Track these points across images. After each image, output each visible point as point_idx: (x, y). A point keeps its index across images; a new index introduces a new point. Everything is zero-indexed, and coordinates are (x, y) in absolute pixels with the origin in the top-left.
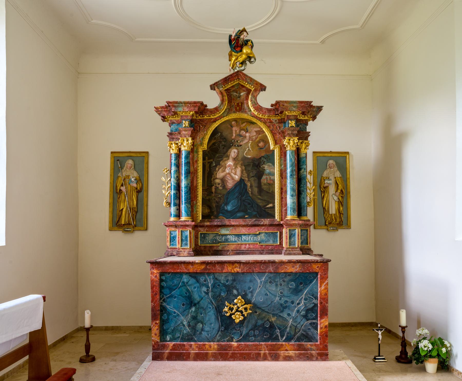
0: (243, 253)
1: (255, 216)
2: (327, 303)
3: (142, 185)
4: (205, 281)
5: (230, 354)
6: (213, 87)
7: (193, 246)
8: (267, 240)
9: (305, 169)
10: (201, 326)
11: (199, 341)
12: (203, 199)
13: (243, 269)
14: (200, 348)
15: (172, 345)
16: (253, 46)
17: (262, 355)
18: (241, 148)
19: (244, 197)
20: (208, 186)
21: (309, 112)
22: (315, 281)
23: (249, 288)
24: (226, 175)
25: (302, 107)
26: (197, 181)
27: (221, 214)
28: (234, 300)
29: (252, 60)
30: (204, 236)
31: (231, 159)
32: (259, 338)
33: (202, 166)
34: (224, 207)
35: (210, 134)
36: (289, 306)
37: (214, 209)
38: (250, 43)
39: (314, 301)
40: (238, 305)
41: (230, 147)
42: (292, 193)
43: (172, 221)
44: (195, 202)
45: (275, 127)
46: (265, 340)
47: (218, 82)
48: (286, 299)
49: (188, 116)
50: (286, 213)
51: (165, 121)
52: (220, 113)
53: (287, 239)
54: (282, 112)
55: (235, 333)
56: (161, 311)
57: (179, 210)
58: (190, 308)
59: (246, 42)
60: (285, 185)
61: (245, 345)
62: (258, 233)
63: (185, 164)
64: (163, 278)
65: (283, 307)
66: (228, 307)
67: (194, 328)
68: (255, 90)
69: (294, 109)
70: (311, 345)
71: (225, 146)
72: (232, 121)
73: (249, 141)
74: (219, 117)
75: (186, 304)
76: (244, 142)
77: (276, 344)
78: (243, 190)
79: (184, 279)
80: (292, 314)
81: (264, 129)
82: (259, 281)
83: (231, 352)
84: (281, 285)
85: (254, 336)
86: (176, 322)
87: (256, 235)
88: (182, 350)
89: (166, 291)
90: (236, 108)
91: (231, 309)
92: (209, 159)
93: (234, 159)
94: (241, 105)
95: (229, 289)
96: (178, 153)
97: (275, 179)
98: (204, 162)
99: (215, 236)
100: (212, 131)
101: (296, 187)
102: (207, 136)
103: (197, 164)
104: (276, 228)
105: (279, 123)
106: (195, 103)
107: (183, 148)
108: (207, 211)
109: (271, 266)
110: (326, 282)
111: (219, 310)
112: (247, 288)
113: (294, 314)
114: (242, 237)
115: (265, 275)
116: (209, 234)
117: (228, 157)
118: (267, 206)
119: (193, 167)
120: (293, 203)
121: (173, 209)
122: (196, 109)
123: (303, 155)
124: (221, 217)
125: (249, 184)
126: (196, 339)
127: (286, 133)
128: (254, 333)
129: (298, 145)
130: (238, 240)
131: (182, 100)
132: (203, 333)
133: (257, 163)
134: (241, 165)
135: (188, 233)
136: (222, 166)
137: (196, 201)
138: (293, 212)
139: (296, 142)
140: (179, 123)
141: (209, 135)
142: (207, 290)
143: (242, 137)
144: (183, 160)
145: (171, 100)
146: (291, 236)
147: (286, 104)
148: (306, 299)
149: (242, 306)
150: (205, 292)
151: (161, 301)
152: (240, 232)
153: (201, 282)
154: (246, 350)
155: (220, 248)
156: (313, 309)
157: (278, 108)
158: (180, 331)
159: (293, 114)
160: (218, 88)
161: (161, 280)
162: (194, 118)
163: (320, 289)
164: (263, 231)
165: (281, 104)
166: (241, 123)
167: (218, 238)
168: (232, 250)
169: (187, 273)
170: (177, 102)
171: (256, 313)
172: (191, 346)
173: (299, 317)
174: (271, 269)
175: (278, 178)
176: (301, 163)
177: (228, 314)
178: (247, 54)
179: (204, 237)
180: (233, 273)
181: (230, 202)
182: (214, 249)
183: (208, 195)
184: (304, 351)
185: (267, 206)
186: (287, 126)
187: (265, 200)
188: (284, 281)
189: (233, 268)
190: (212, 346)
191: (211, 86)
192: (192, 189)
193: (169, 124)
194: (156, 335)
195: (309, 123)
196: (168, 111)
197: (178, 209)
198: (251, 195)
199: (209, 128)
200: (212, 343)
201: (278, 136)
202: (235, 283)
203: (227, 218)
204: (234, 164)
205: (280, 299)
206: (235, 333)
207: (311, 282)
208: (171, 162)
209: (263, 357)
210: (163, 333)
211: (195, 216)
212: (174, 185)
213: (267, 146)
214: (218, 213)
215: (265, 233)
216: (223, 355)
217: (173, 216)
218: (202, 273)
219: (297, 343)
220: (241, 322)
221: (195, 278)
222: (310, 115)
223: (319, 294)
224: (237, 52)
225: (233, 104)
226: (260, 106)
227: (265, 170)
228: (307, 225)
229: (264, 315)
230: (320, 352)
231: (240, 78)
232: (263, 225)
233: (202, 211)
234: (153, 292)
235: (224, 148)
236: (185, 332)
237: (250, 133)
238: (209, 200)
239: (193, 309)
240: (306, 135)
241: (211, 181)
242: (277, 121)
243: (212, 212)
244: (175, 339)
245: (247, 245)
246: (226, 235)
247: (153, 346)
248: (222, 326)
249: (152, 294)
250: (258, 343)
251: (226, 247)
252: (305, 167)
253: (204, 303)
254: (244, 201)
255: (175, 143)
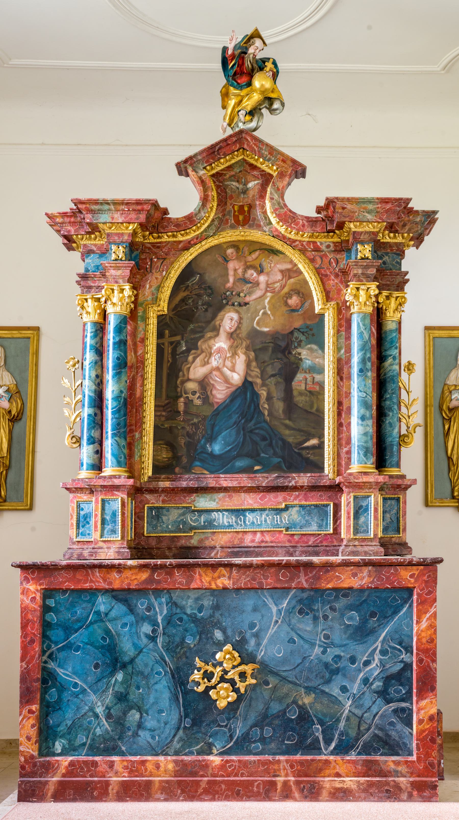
0: (247, 552)
1: (277, 468)
2: (434, 661)
3: (23, 404)
4: (149, 609)
5: (203, 785)
6: (183, 168)
7: (130, 535)
8: (303, 522)
9: (394, 358)
10: (137, 716)
11: (131, 754)
12: (156, 427)
13: (238, 580)
14: (132, 769)
15: (66, 764)
16: (278, 72)
17: (279, 786)
18: (248, 310)
19: (253, 422)
20: (168, 397)
21: (404, 225)
22: (405, 609)
23: (252, 626)
24: (211, 373)
25: (387, 211)
26: (143, 385)
27: (198, 463)
28: (215, 653)
29: (276, 105)
30: (157, 514)
31: (223, 335)
32: (273, 745)
33: (155, 351)
34: (204, 447)
36: (344, 668)
37: (183, 452)
38: (269, 65)
39: (404, 656)
40: (225, 665)
41: (220, 308)
42: (363, 411)
43: (82, 479)
44: (137, 435)
45: (326, 261)
46: (288, 751)
47: (195, 155)
48: (337, 651)
49: (122, 234)
50: (349, 459)
51: (73, 249)
52: (198, 228)
53: (349, 518)
54: (341, 226)
55: (216, 733)
56: (44, 681)
57: (100, 453)
58: (112, 674)
59: (261, 65)
60: (348, 394)
61: (240, 761)
62: (283, 506)
63: (117, 344)
64: (51, 603)
65: (331, 671)
66: (202, 672)
67: (119, 722)
68: (281, 175)
69: (369, 217)
70: (397, 763)
71: (209, 305)
72: (228, 248)
73: (264, 294)
75: (104, 663)
76: (254, 296)
77: (312, 760)
78: (249, 407)
79: (100, 604)
80: (352, 688)
81: (300, 266)
82: (274, 609)
83: (206, 779)
84: (326, 617)
85: (263, 740)
86: (78, 708)
87: (279, 511)
88: (91, 776)
89: (56, 634)
90: (236, 218)
91: (208, 676)
93: (231, 336)
94: (249, 211)
95: (204, 628)
96: (101, 320)
97: (324, 382)
98: (161, 341)
99: (184, 514)
100: (180, 270)
101: (372, 399)
103: (145, 346)
105: (335, 251)
106: (139, 202)
107: (110, 309)
108: (165, 455)
109: (302, 574)
110: (432, 610)
111: (180, 679)
112: (246, 627)
113: (355, 688)
114: (245, 516)
115: (288, 594)
116: (168, 509)
117: (216, 330)
118: (306, 444)
119: (136, 352)
120: (365, 434)
121: (86, 452)
122: (142, 217)
123: (390, 326)
124: (197, 470)
125: (265, 393)
126: (124, 748)
127: (352, 274)
128: (262, 733)
129: (378, 303)
130: (238, 524)
131: (109, 196)
132: (140, 733)
134: (247, 348)
135: (117, 505)
136: (202, 352)
137: (141, 433)
138: (365, 455)
139: (372, 293)
140: (104, 252)
141: (174, 280)
142: (154, 631)
143: (250, 285)
144: (111, 336)
145: (83, 197)
146: (359, 511)
147: (349, 206)
148: (383, 652)
149: (234, 667)
150: (147, 636)
151: (45, 658)
152: (241, 505)
153: (140, 612)
154: (242, 775)
155: (194, 542)
156: (401, 676)
157: (332, 215)
158: (88, 730)
159: (367, 229)
160: (194, 170)
161: (46, 609)
162: (139, 239)
163: (418, 629)
164: (296, 502)
165: (339, 204)
166: (247, 253)
167: (190, 519)
168: (222, 547)
169: (106, 591)
170: (96, 202)
171: (267, 683)
172: (111, 765)
173: (367, 694)
174: (303, 580)
175: (331, 377)
176: (387, 345)
177: (201, 689)
178: (263, 91)
179: (158, 517)
180: (214, 590)
182: (179, 544)
183: (168, 419)
184: (379, 776)
185: (306, 444)
186: (353, 257)
187: (300, 430)
188: (333, 609)
189: (214, 579)
190: (162, 765)
191: (178, 165)
192: (130, 405)
193: (83, 255)
194: (29, 738)
195: (406, 252)
196: (77, 224)
197: (97, 452)
198: (268, 419)
199: (173, 263)
200: (161, 758)
201: (333, 282)
202: (217, 615)
203: (211, 472)
204: (231, 347)
205: (324, 652)
206: (216, 733)
207: (396, 612)
208: (84, 343)
209: (282, 791)
210: (46, 735)
211: (136, 467)
212: (89, 396)
213: (307, 304)
214: (192, 460)
215: (301, 506)
216: (187, 786)
217: (85, 466)
218: (141, 591)
219: (364, 757)
220: (232, 707)
221: (125, 601)
222: (408, 233)
223: (415, 639)
224: (240, 87)
226: (290, 211)
227: (301, 359)
228: (399, 486)
229: (285, 690)
230: (418, 779)
231: (245, 146)
232: (295, 488)
233: (154, 456)
234: (24, 635)
235: (206, 310)
236: (98, 731)
237: (268, 274)
238: (171, 429)
239: (120, 676)
240: (399, 279)
241: (176, 387)
242: (332, 248)
243: (176, 458)
244: (74, 750)
245: (259, 535)
246: (209, 511)
247: (23, 767)
248: (186, 716)
249: (22, 642)
250: (270, 758)
251: (207, 538)
252: (395, 352)
253: (146, 661)
254: (251, 431)
255: (92, 298)
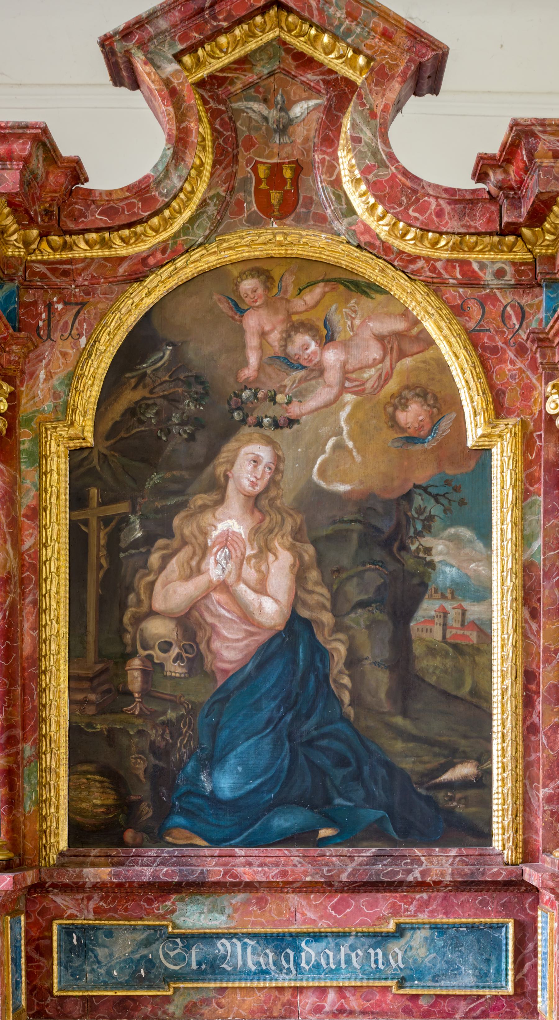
1: (375, 833)
8: (441, 965)
19: (314, 720)
20: (101, 656)
24: (206, 596)
26: (38, 626)
27: (179, 820)
30: (82, 944)
31: (234, 501)
33: (65, 540)
34: (194, 780)
35: (113, 350)
37: (142, 791)
41: (228, 431)
44: (28, 750)
45: (494, 311)
62: (391, 927)
71: (198, 423)
72: (243, 276)
74: (163, 248)
76: (312, 403)
78: (304, 680)
81: (429, 326)
87: (381, 939)
92: (103, 503)
93: (255, 502)
97: (490, 622)
98: (80, 515)
99: (147, 943)
100: (122, 334)
102: (94, 362)
103: (40, 527)
104: (495, 901)
105: (518, 286)
108: (99, 799)
114: (298, 950)
117: (218, 488)
118: (447, 776)
124: (179, 836)
133: (386, 526)
134: (297, 535)
136: (185, 543)
137: (37, 744)
141: (107, 360)
143: (302, 373)
164: (423, 918)
166: (291, 290)
167: (165, 956)
181: (230, 747)
183: (103, 710)
185: (447, 776)
187: (430, 742)
198: (350, 712)
199: (103, 315)
201: (511, 367)
203: (214, 843)
204: (255, 532)
213: (445, 424)
214: (164, 812)
215: (434, 927)
225: (244, 170)
226: (406, 173)
227: (431, 564)
235: (192, 437)
237: (346, 345)
238: (111, 737)
241: (122, 631)
242: (510, 278)
243: (126, 807)
245: (332, 996)
246: (209, 938)
251: (206, 1002)
254: (310, 743)
